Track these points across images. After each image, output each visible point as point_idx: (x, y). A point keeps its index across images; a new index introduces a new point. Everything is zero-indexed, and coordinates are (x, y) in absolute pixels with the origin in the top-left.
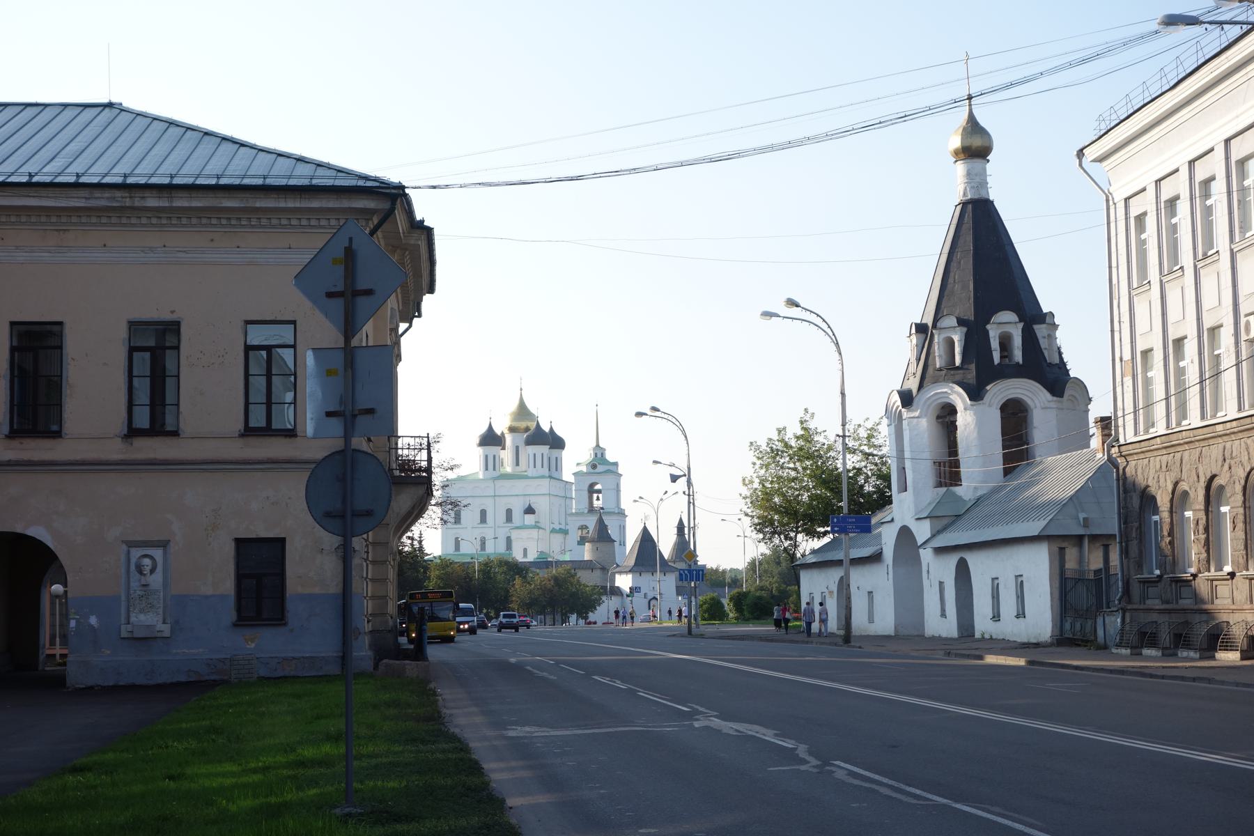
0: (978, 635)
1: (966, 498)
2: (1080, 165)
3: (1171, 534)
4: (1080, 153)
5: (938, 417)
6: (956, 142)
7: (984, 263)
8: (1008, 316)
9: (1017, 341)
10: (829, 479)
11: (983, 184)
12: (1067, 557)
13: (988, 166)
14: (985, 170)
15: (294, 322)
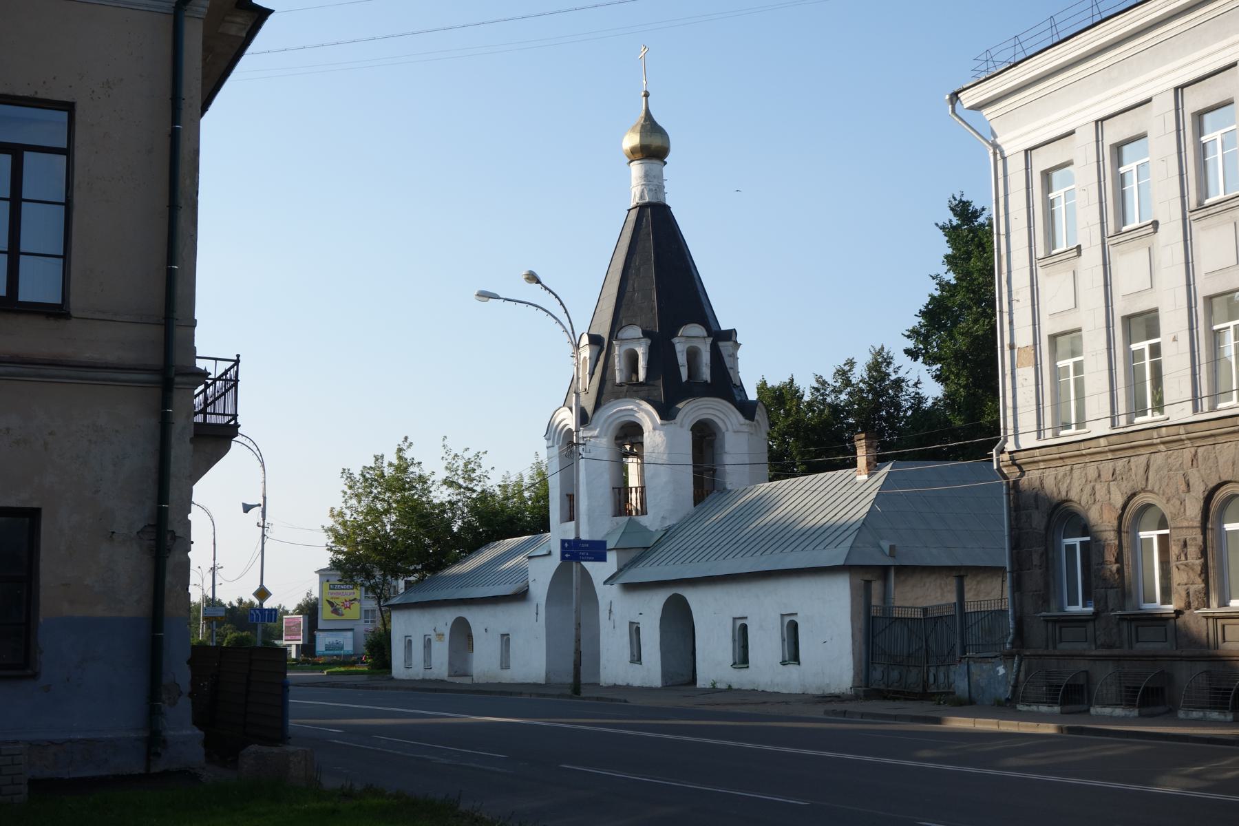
0: (703, 681)
1: (653, 529)
2: (953, 111)
3: (1119, 559)
4: (955, 96)
5: (617, 438)
6: (632, 140)
7: (659, 273)
8: (696, 330)
9: (706, 357)
10: (422, 517)
11: (660, 189)
12: (966, 589)
13: (665, 169)
14: (661, 171)
15: (69, 107)
